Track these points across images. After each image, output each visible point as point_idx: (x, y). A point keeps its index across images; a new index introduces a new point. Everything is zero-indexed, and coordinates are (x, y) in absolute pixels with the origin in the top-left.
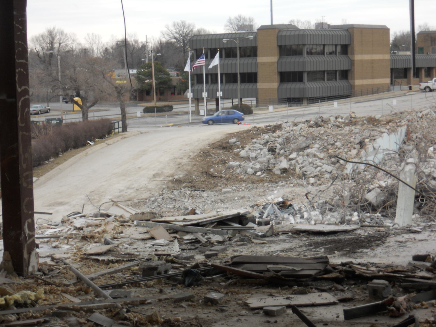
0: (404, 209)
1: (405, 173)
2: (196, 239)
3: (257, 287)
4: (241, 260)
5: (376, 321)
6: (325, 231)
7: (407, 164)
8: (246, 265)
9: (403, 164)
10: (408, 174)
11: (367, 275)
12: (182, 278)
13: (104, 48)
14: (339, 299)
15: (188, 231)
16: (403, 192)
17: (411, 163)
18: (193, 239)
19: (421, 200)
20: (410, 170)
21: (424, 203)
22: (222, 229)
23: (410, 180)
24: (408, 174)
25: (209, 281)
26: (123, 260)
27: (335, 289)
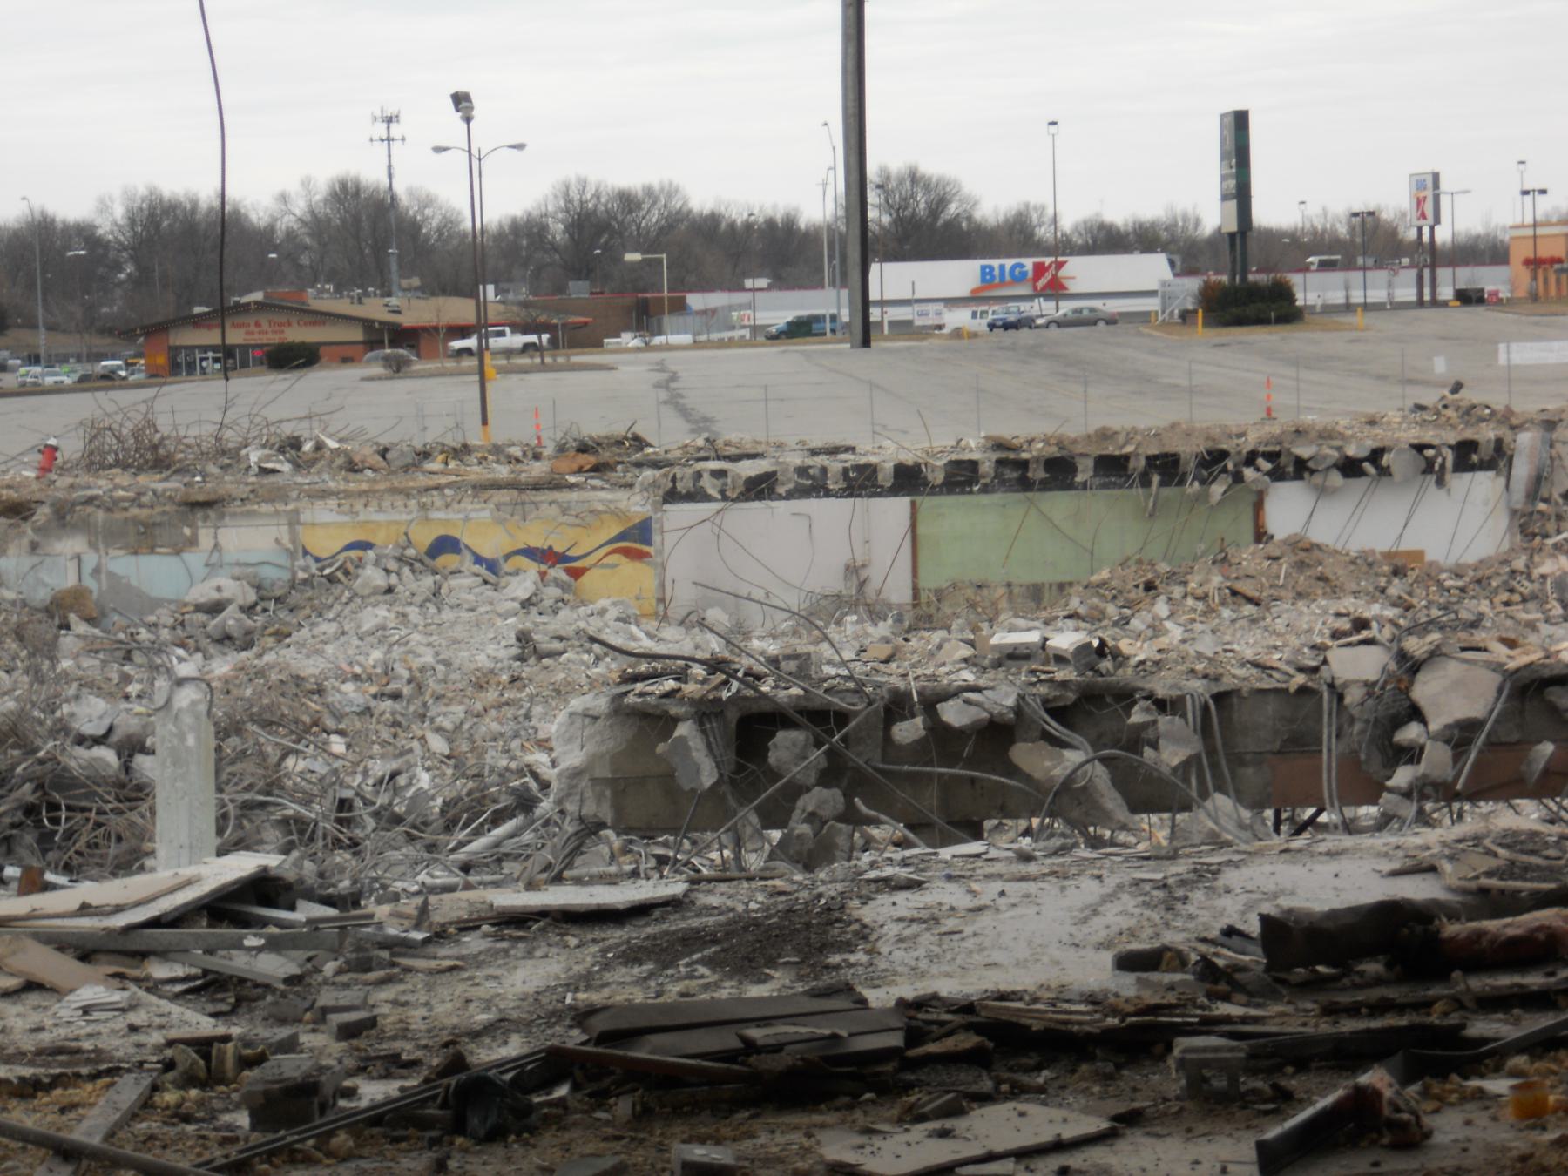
0: (191, 847)
1: (176, 717)
2: (206, 972)
3: (752, 1111)
4: (623, 1024)
5: (1376, 1164)
6: (621, 907)
7: (181, 682)
8: (656, 1039)
9: (162, 683)
10: (188, 719)
11: (1087, 1028)
12: (448, 1113)
13: (788, 216)
14: (1113, 1113)
15: (143, 948)
16: (179, 784)
17: (193, 679)
18: (195, 978)
19: (50, 820)
20: (193, 703)
21: (61, 829)
22: (317, 929)
23: (198, 739)
24: (188, 719)
25: (554, 1111)
26: (78, 1076)
27: (1012, 1087)
